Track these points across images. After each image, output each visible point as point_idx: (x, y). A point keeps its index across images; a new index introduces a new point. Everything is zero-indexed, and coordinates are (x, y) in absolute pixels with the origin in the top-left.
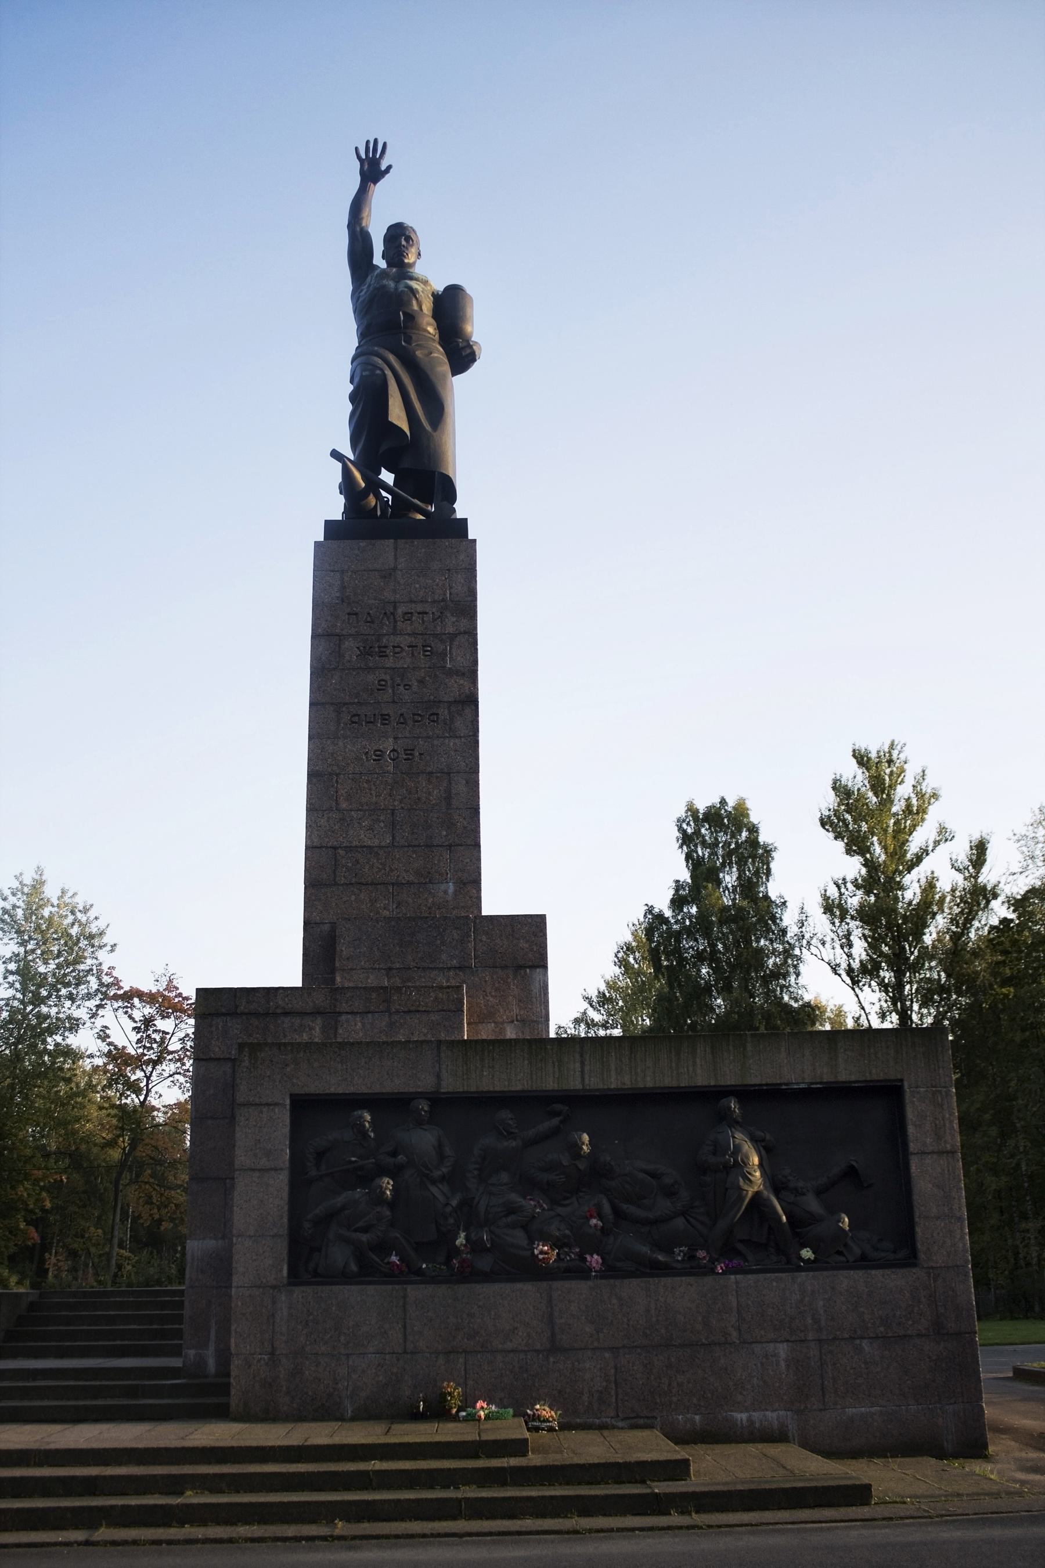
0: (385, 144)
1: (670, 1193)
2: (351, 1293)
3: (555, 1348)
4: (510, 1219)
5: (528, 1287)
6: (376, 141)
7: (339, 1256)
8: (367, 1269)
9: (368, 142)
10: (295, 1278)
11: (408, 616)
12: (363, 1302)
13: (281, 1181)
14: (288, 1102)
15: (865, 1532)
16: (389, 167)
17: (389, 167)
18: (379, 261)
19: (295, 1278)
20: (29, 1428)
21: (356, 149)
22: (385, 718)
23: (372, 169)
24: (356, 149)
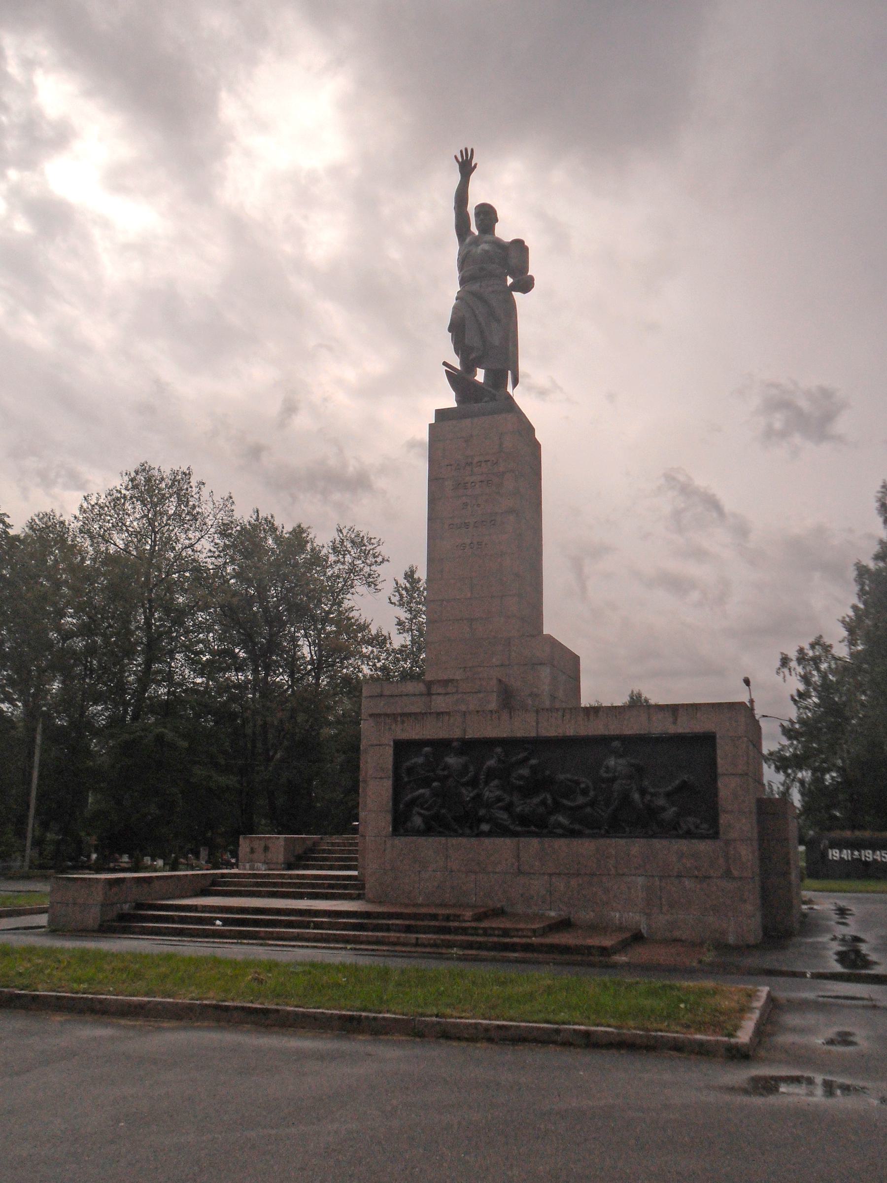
0: (472, 150)
1: (585, 792)
2: (421, 840)
3: (520, 872)
4: (500, 804)
5: (508, 841)
6: (466, 150)
7: (418, 821)
8: (428, 831)
9: (461, 152)
10: (396, 832)
11: (479, 463)
12: (429, 845)
13: (388, 784)
14: (392, 743)
15: (24, 938)
16: (476, 165)
17: (476, 165)
18: (474, 229)
19: (396, 832)
20: (216, 898)
21: (456, 157)
22: (467, 525)
23: (466, 167)
24: (456, 157)
